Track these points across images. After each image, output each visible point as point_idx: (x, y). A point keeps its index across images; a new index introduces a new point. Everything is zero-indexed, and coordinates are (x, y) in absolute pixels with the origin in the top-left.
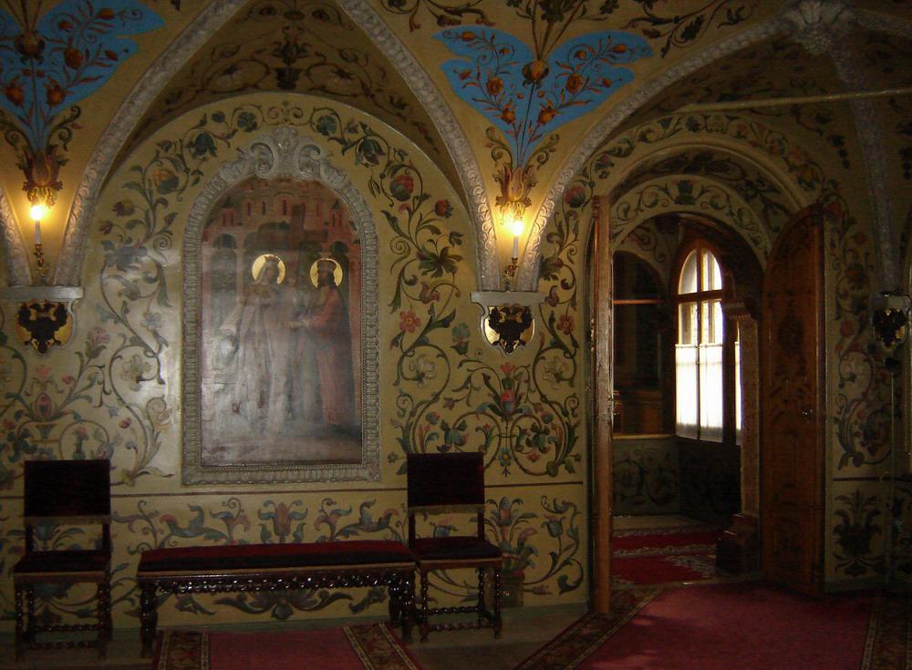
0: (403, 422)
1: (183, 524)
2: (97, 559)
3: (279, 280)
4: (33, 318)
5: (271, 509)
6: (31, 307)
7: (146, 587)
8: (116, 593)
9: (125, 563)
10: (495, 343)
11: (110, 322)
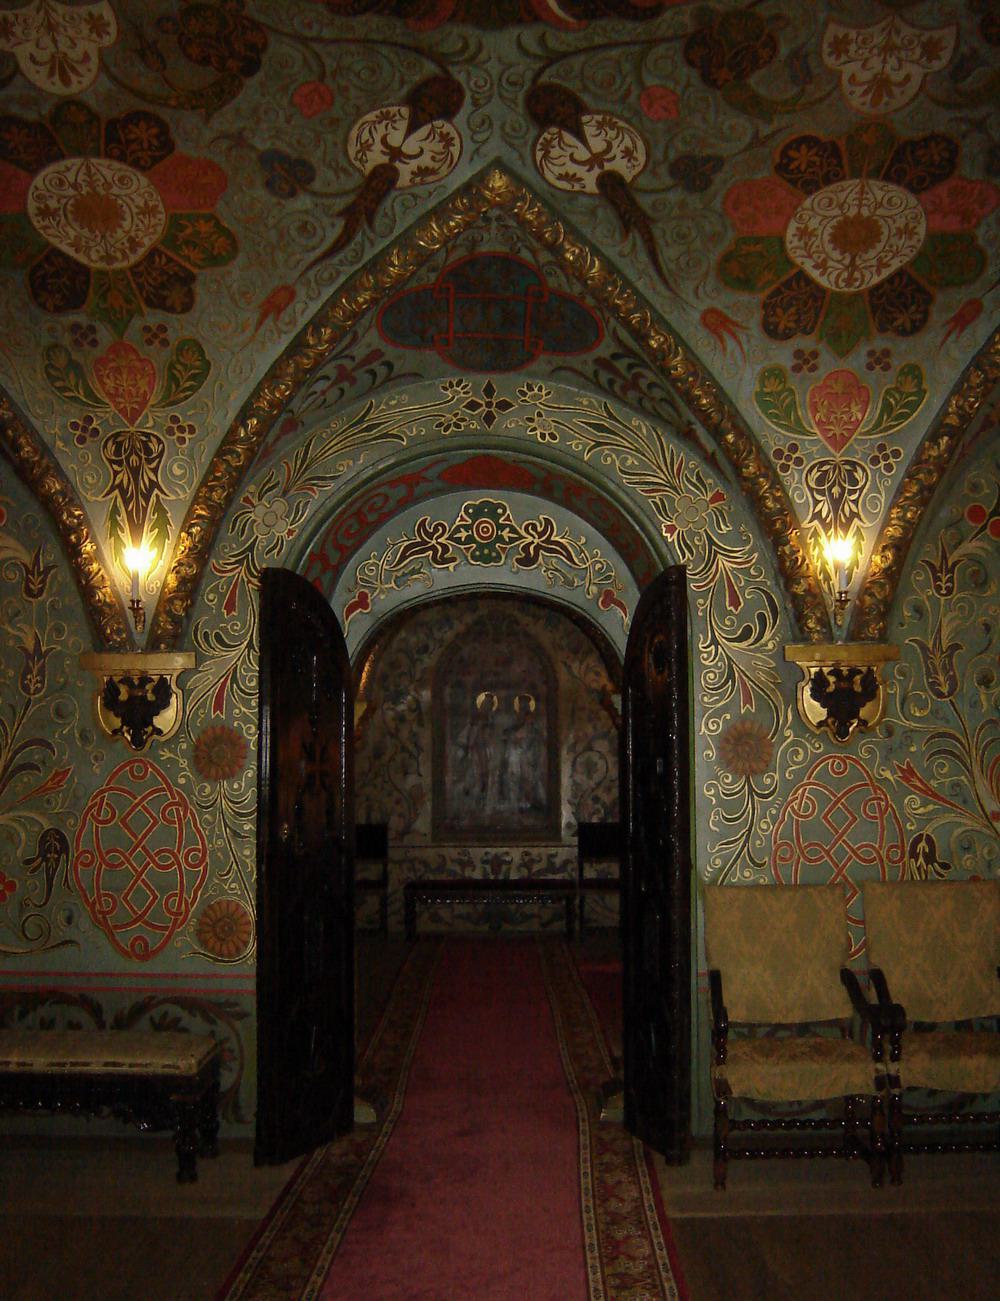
0: (576, 801)
1: (433, 866)
2: (382, 883)
3: (494, 709)
4: (124, 696)
5: (490, 857)
6: (121, 681)
7: (409, 905)
8: (390, 909)
9: (395, 887)
10: (821, 724)
11: (388, 737)
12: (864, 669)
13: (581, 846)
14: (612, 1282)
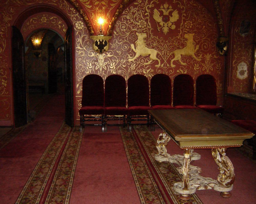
12: (105, 41)
13: (82, 105)
14: (128, 146)
